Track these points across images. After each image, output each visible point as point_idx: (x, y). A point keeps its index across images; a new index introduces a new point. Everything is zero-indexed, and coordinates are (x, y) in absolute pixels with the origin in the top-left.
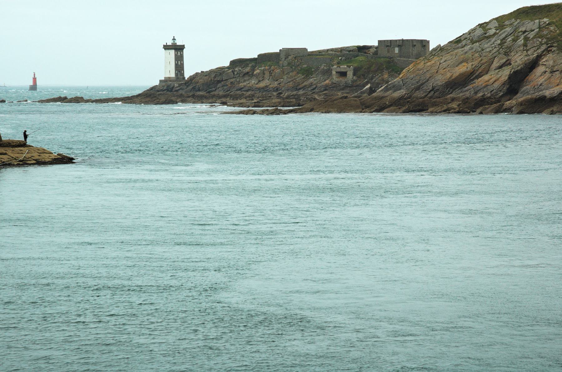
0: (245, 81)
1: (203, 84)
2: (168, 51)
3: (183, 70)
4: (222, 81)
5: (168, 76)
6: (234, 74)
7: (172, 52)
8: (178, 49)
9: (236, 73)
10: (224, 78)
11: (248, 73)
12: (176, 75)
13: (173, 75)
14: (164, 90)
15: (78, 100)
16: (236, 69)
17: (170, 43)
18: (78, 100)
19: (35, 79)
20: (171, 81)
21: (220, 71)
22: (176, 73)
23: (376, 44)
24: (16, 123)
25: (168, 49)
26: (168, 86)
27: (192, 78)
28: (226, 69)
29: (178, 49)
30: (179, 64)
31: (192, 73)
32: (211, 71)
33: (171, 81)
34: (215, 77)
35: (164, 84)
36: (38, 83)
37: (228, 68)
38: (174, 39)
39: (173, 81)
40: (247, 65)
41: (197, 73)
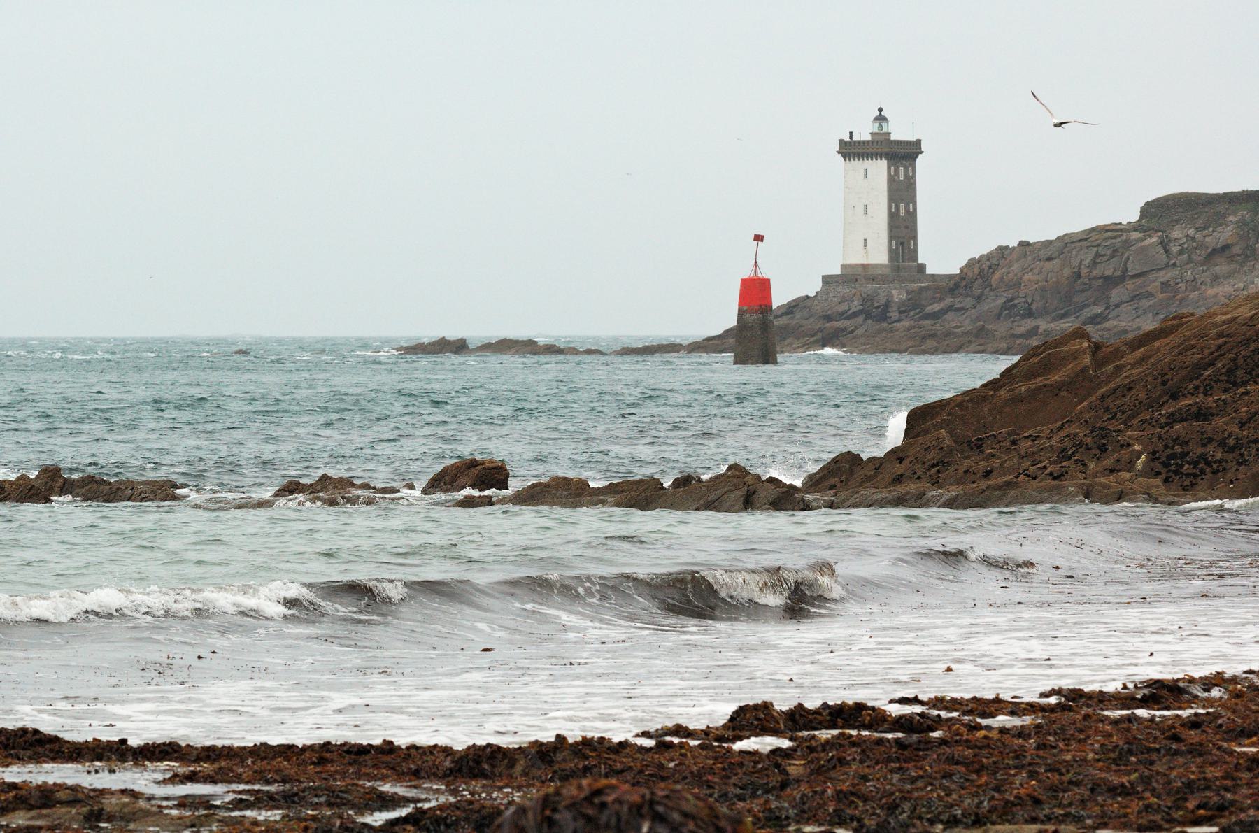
0: (1216, 279)
1: (1043, 289)
2: (859, 165)
3: (915, 238)
4: (1123, 278)
5: (857, 259)
6: (1167, 251)
7: (879, 169)
8: (902, 155)
9: (1175, 249)
10: (1133, 268)
11: (1225, 248)
14: (854, 315)
15: (559, 351)
16: (1177, 233)
17: (864, 132)
18: (551, 350)
20: (873, 279)
21: (1104, 241)
22: (890, 251)
23: (920, 261)
24: (364, 357)
26: (867, 300)
28: (1135, 235)
29: (902, 155)
32: (1067, 243)
33: (873, 279)
34: (1094, 263)
35: (844, 291)
37: (1135, 227)
38: (881, 118)
39: (884, 279)
40: (1219, 220)
41: (1002, 250)
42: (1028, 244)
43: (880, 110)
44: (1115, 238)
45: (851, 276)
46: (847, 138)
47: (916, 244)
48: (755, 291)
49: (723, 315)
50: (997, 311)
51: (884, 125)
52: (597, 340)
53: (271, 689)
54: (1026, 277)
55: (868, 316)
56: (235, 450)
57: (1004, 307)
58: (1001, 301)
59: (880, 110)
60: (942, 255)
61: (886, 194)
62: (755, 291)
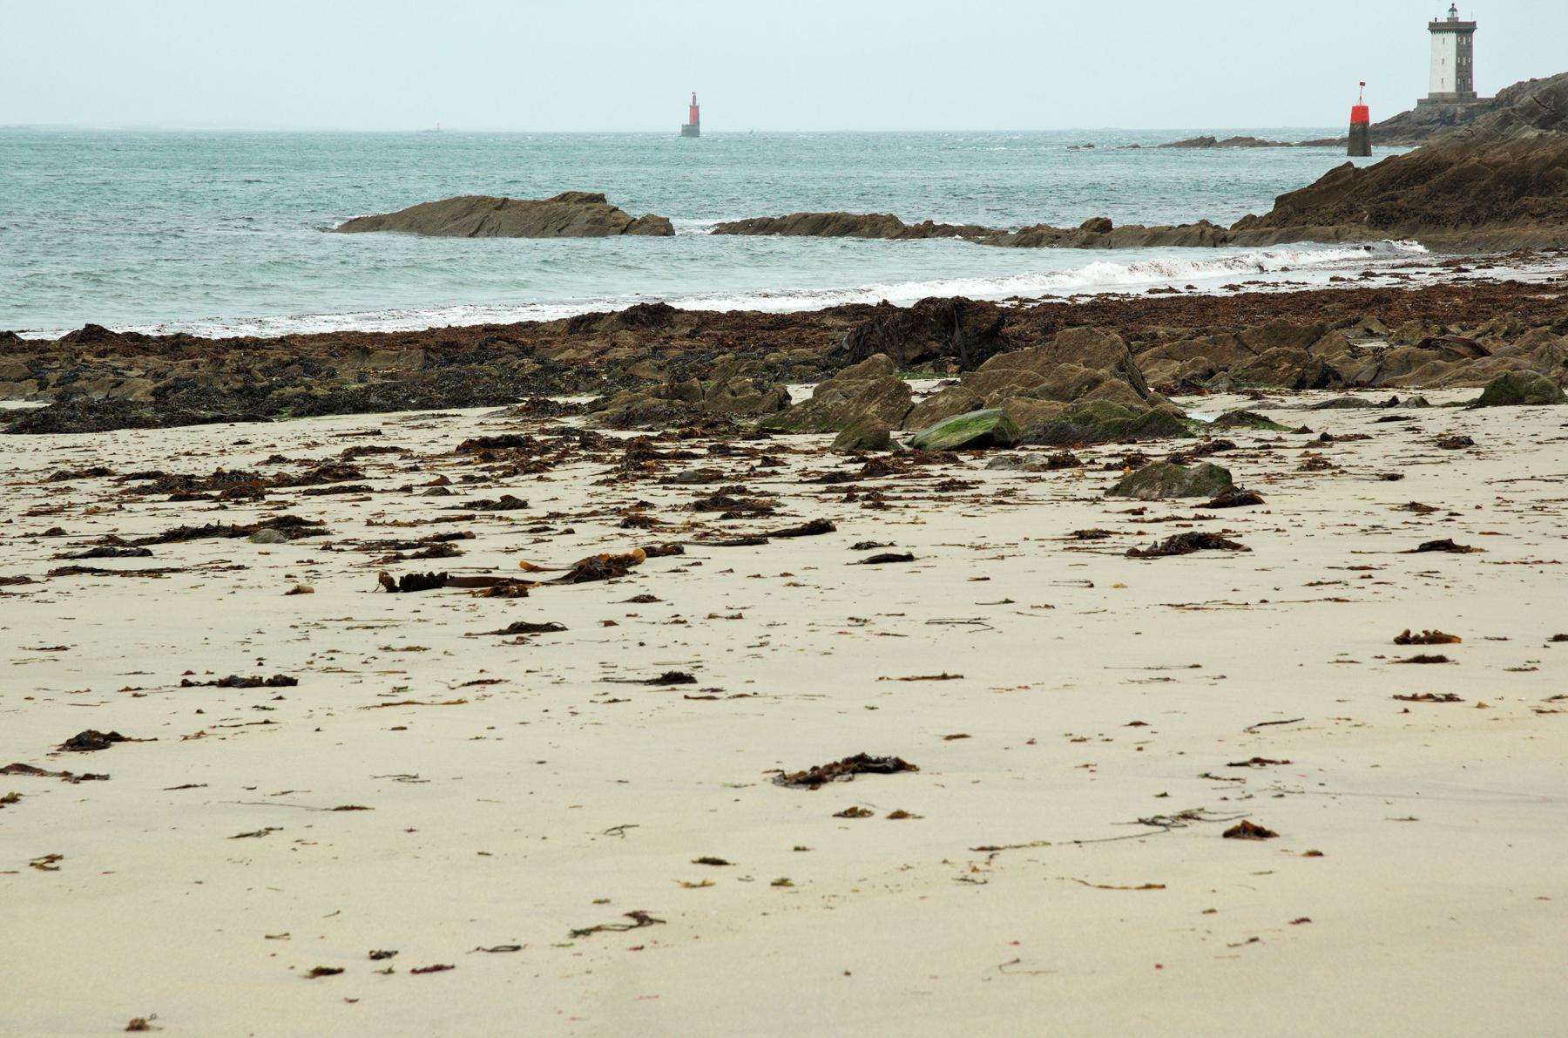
2: (1440, 36)
5: (1438, 89)
7: (1451, 38)
8: (1464, 30)
12: (1458, 87)
13: (1450, 87)
17: (1443, 18)
19: (695, 110)
25: (1440, 31)
26: (1442, 113)
27: (1507, 96)
29: (1464, 30)
35: (1430, 108)
38: (1453, 10)
45: (1434, 100)
48: (1360, 113)
49: (1341, 125)
55: (1443, 122)
56: (116, 393)
60: (1486, 86)
62: (1360, 113)
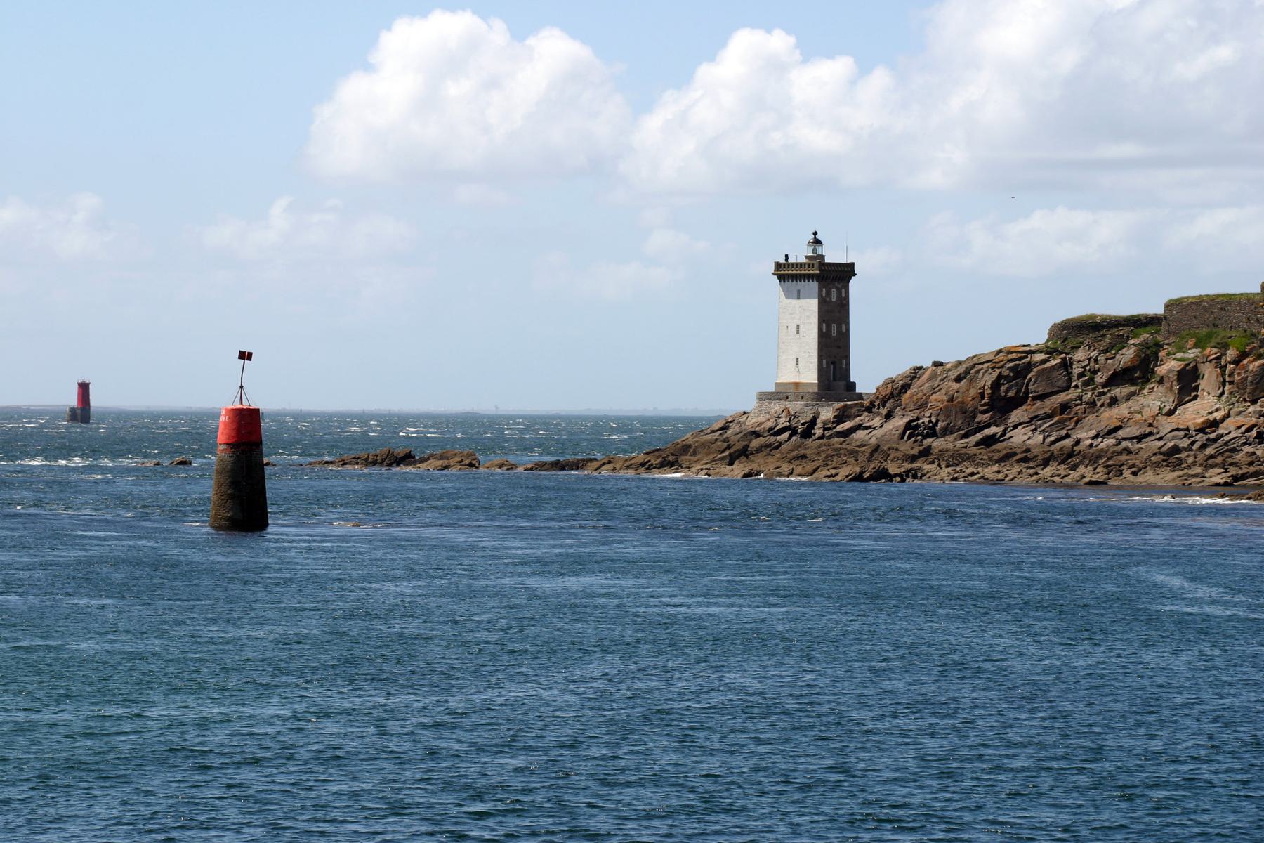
3: (847, 357)
16: (1080, 355)
17: (799, 255)
19: (84, 388)
27: (895, 392)
30: (834, 333)
31: (898, 368)
36: (96, 401)
40: (1121, 343)
42: (941, 364)
43: (815, 234)
44: (1020, 359)
46: (782, 260)
47: (848, 364)
50: (900, 431)
51: (819, 248)
52: (392, 422)
53: (1080, 806)
54: (933, 397)
57: (908, 426)
58: (906, 420)
59: (815, 234)
61: (816, 314)
